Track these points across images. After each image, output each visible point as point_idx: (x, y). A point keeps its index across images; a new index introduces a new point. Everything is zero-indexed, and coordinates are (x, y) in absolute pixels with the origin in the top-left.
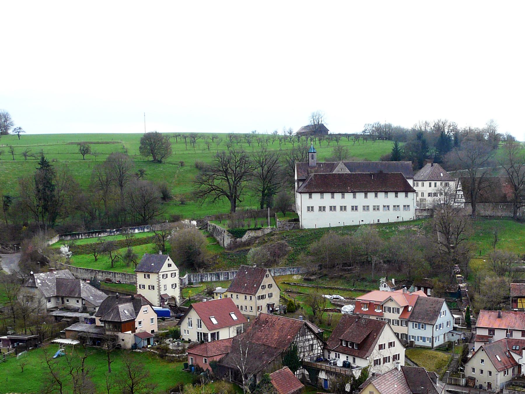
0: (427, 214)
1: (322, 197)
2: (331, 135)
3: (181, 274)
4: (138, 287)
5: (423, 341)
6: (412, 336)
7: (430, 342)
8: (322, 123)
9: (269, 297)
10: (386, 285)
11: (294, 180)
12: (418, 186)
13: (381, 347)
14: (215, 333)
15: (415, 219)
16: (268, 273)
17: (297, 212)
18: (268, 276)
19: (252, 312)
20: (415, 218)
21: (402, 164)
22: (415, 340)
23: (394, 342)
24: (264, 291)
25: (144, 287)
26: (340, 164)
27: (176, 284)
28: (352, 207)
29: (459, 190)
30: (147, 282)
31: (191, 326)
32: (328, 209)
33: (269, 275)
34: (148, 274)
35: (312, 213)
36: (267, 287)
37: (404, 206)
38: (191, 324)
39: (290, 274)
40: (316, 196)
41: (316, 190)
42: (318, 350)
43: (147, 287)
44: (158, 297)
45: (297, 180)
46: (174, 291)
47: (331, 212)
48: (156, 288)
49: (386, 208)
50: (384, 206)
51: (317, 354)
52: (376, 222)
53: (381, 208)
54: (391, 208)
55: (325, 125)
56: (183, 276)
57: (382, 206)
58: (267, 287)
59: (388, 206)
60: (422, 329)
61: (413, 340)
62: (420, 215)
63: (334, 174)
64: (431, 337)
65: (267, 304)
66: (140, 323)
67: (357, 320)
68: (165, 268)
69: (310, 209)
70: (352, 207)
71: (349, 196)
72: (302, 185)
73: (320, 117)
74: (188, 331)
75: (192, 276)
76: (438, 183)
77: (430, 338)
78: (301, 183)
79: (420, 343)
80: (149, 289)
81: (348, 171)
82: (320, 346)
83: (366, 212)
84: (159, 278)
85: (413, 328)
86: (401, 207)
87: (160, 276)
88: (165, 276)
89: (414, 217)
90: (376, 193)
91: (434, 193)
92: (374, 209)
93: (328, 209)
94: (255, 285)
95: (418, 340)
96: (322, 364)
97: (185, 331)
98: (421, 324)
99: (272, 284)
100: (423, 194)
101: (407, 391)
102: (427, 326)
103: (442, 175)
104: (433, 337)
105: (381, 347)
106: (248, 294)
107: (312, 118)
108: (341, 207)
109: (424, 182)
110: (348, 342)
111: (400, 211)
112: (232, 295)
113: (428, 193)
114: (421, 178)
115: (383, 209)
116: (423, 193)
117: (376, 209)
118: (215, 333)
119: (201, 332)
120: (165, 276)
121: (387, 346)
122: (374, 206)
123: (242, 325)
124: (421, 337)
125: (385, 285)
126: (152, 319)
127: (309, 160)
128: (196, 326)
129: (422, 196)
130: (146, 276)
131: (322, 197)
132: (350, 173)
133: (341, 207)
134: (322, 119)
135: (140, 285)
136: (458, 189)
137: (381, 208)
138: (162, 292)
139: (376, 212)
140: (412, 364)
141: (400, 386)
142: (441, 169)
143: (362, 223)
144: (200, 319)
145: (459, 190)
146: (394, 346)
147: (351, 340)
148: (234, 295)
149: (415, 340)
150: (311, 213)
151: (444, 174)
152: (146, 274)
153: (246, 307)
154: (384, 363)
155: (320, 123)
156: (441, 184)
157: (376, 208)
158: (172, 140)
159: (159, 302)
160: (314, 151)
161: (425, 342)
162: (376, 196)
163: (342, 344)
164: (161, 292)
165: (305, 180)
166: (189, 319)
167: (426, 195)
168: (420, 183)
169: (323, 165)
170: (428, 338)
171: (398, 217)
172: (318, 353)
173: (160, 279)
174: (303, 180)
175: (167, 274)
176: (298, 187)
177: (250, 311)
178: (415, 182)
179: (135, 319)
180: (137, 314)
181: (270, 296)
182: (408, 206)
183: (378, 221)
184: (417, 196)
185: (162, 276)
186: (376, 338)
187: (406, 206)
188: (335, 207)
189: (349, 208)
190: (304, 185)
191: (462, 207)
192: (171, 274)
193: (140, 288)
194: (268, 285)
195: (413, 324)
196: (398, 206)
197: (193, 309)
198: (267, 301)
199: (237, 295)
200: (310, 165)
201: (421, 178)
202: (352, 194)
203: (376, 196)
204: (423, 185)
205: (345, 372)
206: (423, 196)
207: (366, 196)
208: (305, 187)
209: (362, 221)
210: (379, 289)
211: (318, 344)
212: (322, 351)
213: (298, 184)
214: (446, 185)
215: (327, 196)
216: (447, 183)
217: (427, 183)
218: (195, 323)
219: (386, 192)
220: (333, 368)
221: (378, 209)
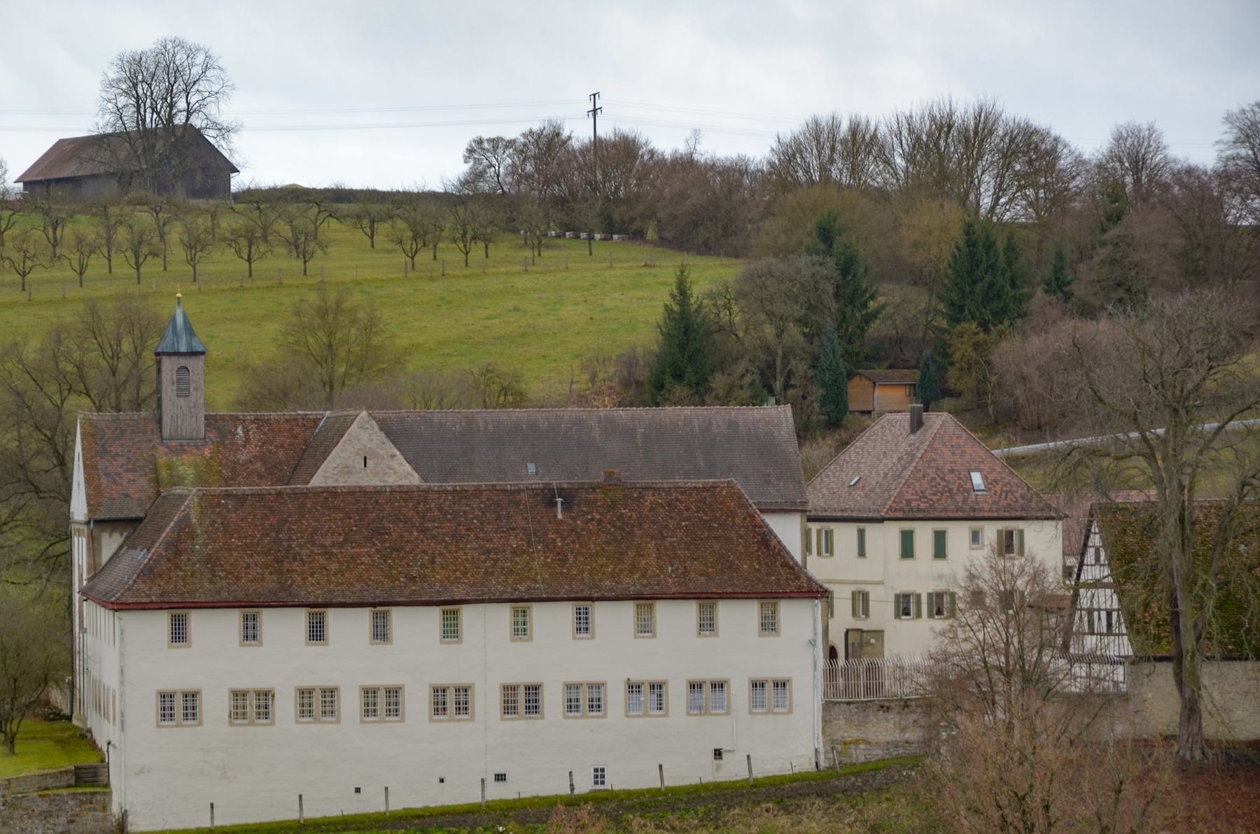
0: (897, 736)
2: (254, 197)
8: (197, 121)
11: (67, 518)
12: (830, 550)
15: (823, 764)
17: (84, 721)
20: (822, 757)
21: (732, 425)
26: (355, 426)
28: (436, 690)
29: (1097, 584)
32: (285, 706)
35: (324, 729)
37: (757, 685)
47: (311, 729)
49: (646, 696)
50: (633, 688)
52: (584, 785)
53: (615, 697)
54: (677, 694)
55: (210, 136)
62: (857, 742)
70: (436, 690)
72: (116, 555)
73: (179, 86)
76: (958, 534)
78: (110, 543)
81: (408, 467)
83: (520, 725)
86: (739, 692)
89: (816, 751)
90: (582, 604)
91: (930, 595)
93: (285, 706)
100: (861, 601)
103: (977, 478)
107: (126, 93)
108: (369, 693)
109: (832, 526)
111: (728, 713)
113: (897, 596)
117: (584, 703)
122: (569, 686)
127: (158, 391)
129: (854, 614)
133: (369, 693)
134: (194, 99)
136: (1089, 574)
137: (615, 697)
139: (585, 725)
142: (968, 449)
143: (497, 792)
145: (1097, 584)
150: (180, 734)
151: (991, 477)
155: (180, 119)
156: (975, 537)
160: (189, 344)
165: (139, 520)
169: (246, 431)
171: (718, 753)
178: (814, 527)
182: (781, 685)
183: (599, 775)
184: (829, 611)
187: (769, 687)
188: (330, 693)
189: (417, 702)
190: (140, 557)
191: (1116, 684)
196: (718, 686)
200: (166, 432)
207: (521, 629)
208: (147, 573)
209: (500, 778)
213: (94, 548)
214: (1008, 544)
216: (1010, 534)
217: (885, 538)
221: (596, 705)
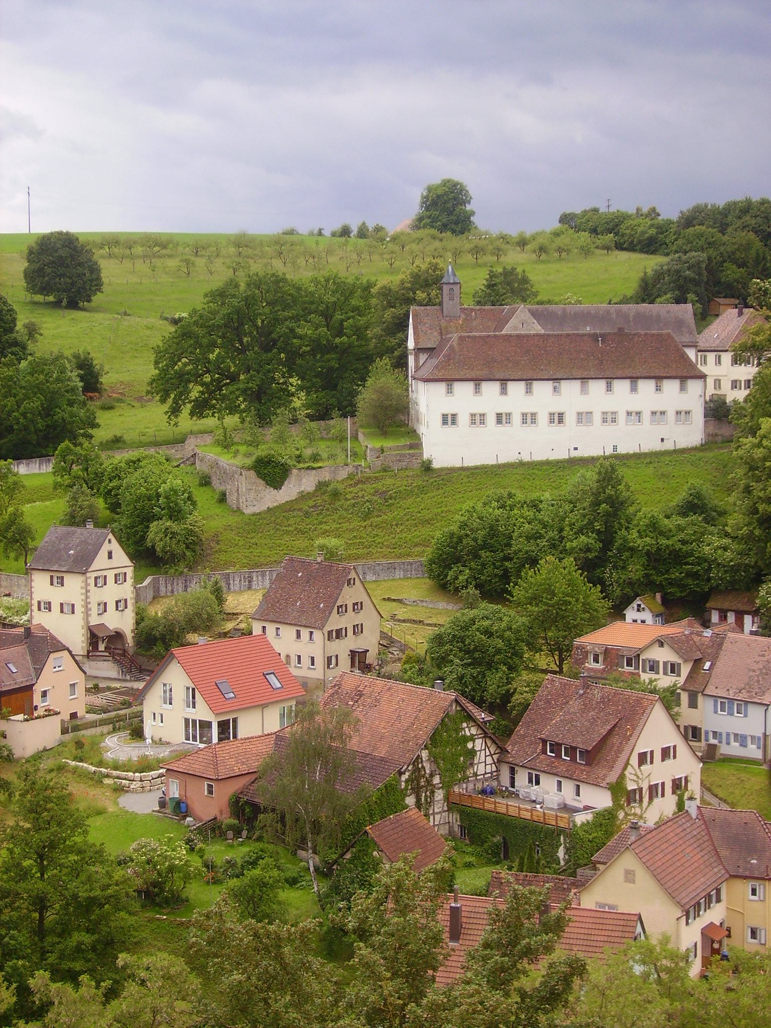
1: (584, 391)
3: (138, 579)
4: (35, 607)
5: (741, 745)
6: (714, 732)
7: (759, 748)
9: (354, 633)
10: (642, 606)
13: (643, 758)
14: (229, 720)
16: (353, 575)
18: (352, 582)
19: (301, 668)
22: (720, 742)
23: (675, 747)
24: (344, 619)
25: (49, 606)
27: (126, 600)
30: (56, 595)
31: (171, 703)
33: (354, 579)
34: (60, 575)
35: (560, 428)
36: (350, 608)
38: (171, 699)
39: (402, 576)
40: (463, 390)
41: (462, 374)
42: (486, 765)
43: (56, 608)
44: (83, 631)
45: (414, 349)
46: (122, 616)
47: (500, 428)
48: (79, 609)
49: (634, 417)
50: (629, 413)
51: (484, 775)
53: (622, 417)
54: (646, 416)
56: (143, 580)
57: (625, 414)
58: (350, 608)
59: (638, 413)
60: (739, 715)
61: (714, 742)
63: (506, 335)
64: (761, 735)
65: (351, 651)
66: (44, 694)
67: (581, 692)
68: (100, 561)
69: (449, 420)
70: (472, 415)
71: (542, 389)
74: (162, 715)
75: (162, 581)
77: (759, 739)
78: (423, 357)
79: (733, 749)
80: (62, 611)
82: (491, 755)
84: (87, 585)
85: (716, 712)
87: (89, 581)
88: (100, 582)
90: (609, 380)
91: (745, 381)
92: (605, 421)
94: (322, 605)
95: (728, 743)
96: (509, 803)
97: (154, 714)
98: (736, 702)
99: (361, 603)
100: (718, 383)
101: (715, 870)
102: (751, 709)
104: (765, 734)
105: (643, 758)
106: (305, 626)
108: (524, 415)
109: (721, 353)
110: (560, 745)
112: (264, 628)
114: (714, 345)
115: (627, 421)
116: (719, 380)
118: (229, 720)
119: (194, 718)
120: (100, 582)
121: (658, 756)
122: (603, 413)
123: (293, 703)
124: (736, 735)
125: (639, 606)
126: (74, 684)
128: (183, 705)
129: (715, 388)
130: (55, 580)
131: (584, 391)
132: (543, 332)
133: (524, 415)
135: (39, 603)
137: (622, 417)
138: (94, 620)
140: (714, 801)
141: (698, 856)
144: (192, 685)
146: (675, 757)
147: (569, 741)
148: (271, 628)
149: (720, 742)
152: (55, 575)
153: (299, 657)
154: (651, 799)
157: (610, 418)
158: (99, 256)
159: (84, 645)
161: (746, 746)
162: (609, 388)
163: (544, 752)
164: (90, 619)
166: (165, 685)
167: (726, 386)
168: (711, 357)
170: (753, 737)
172: (486, 773)
173: (89, 588)
174: (430, 350)
175: (105, 577)
176: (417, 368)
177: (309, 668)
179: (34, 684)
180: (39, 672)
181: (358, 629)
182: (688, 413)
183: (615, 448)
185: (93, 579)
186: (631, 735)
187: (658, 414)
189: (543, 419)
192: (116, 575)
193: (39, 609)
194: (355, 604)
195: (716, 702)
196: (663, 413)
197: (175, 660)
198: (351, 643)
199: (278, 629)
200: (445, 315)
201: (715, 345)
202: (523, 383)
203: (609, 388)
204: (719, 361)
205: (557, 820)
206: (720, 388)
209: (576, 449)
210: (623, 617)
211: (485, 750)
212: (494, 769)
213: (417, 360)
215: (491, 389)
218: (179, 695)
219: (504, 381)
220: (527, 810)
